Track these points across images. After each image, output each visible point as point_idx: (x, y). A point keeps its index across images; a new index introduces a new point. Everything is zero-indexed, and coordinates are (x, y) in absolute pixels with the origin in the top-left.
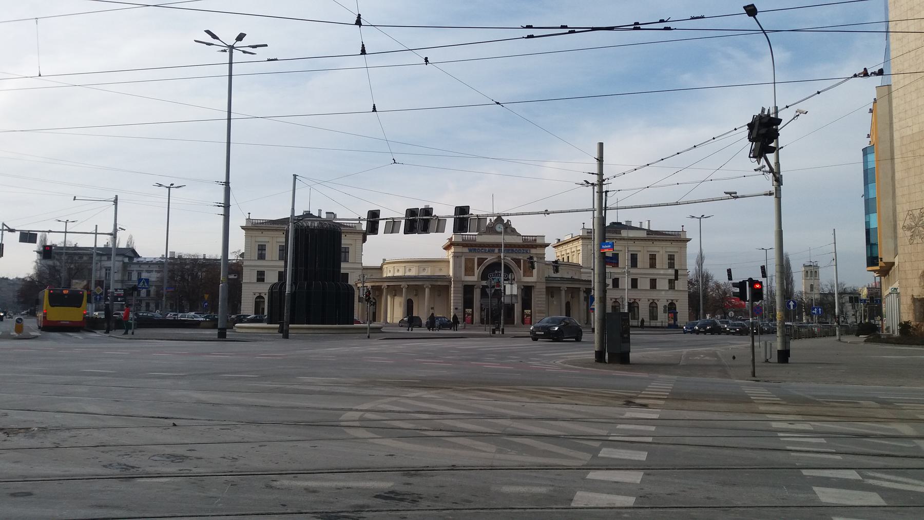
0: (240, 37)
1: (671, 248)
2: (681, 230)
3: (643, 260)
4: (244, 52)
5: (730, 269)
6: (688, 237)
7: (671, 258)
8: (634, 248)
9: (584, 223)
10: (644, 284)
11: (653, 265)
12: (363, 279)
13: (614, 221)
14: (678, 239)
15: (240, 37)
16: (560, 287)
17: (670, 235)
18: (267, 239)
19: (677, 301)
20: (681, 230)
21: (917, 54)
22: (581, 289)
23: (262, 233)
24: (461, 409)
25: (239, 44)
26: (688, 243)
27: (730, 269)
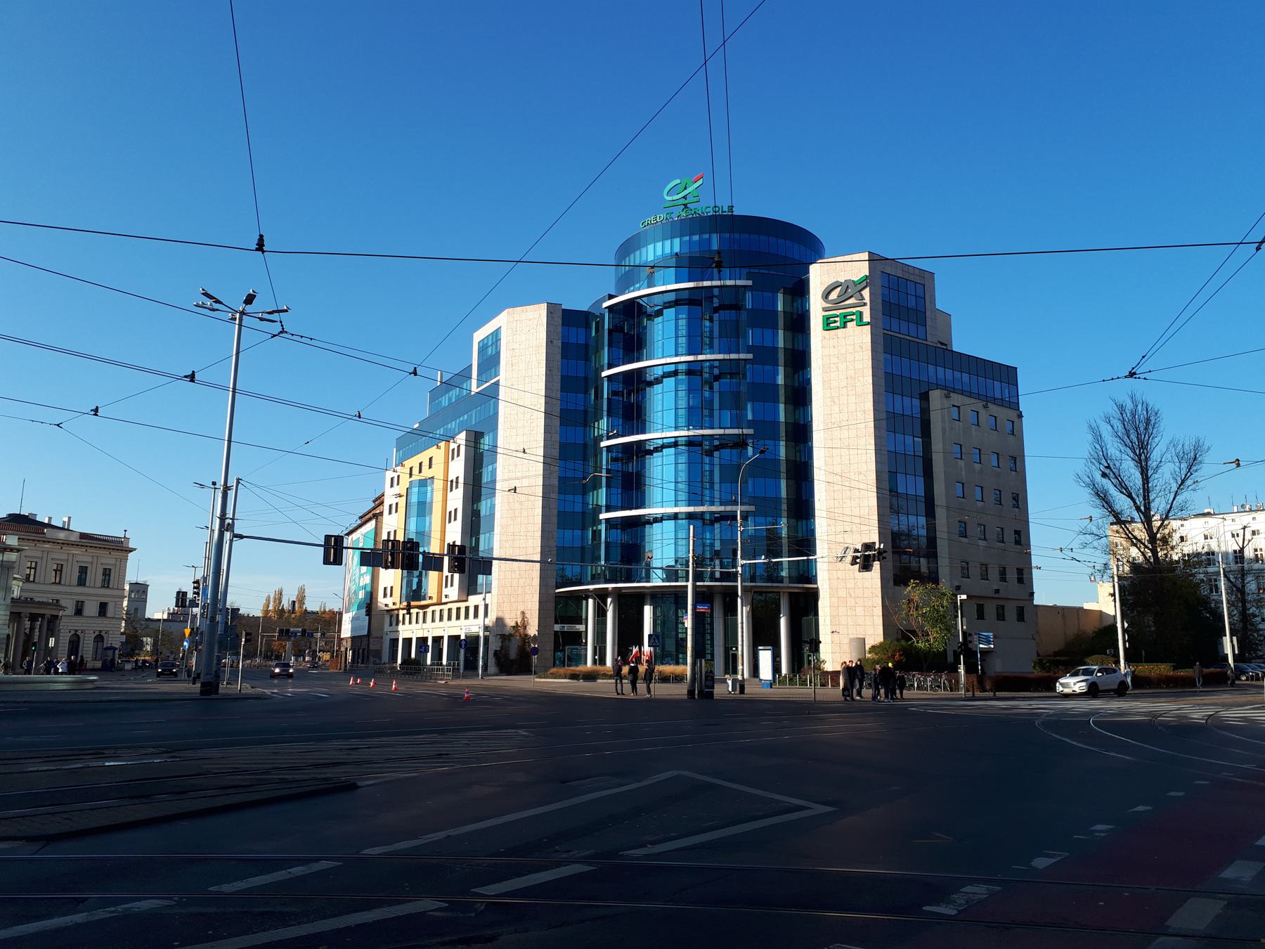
0: (250, 300)
1: (108, 559)
2: (123, 536)
3: (72, 574)
4: (261, 319)
5: (478, 606)
6: (131, 545)
7: (107, 573)
8: (60, 555)
9: (125, 531)
10: (91, 609)
11: (82, 582)
12: (369, 641)
13: (1035, 596)
14: (119, 547)
15: (250, 300)
16: (20, 613)
17: (100, 540)
18: (112, 561)
19: (82, 632)
20: (123, 536)
21: (532, 418)
22: (22, 615)
23: (110, 553)
24: (937, 914)
25: (249, 309)
26: (130, 555)
27: (478, 606)
